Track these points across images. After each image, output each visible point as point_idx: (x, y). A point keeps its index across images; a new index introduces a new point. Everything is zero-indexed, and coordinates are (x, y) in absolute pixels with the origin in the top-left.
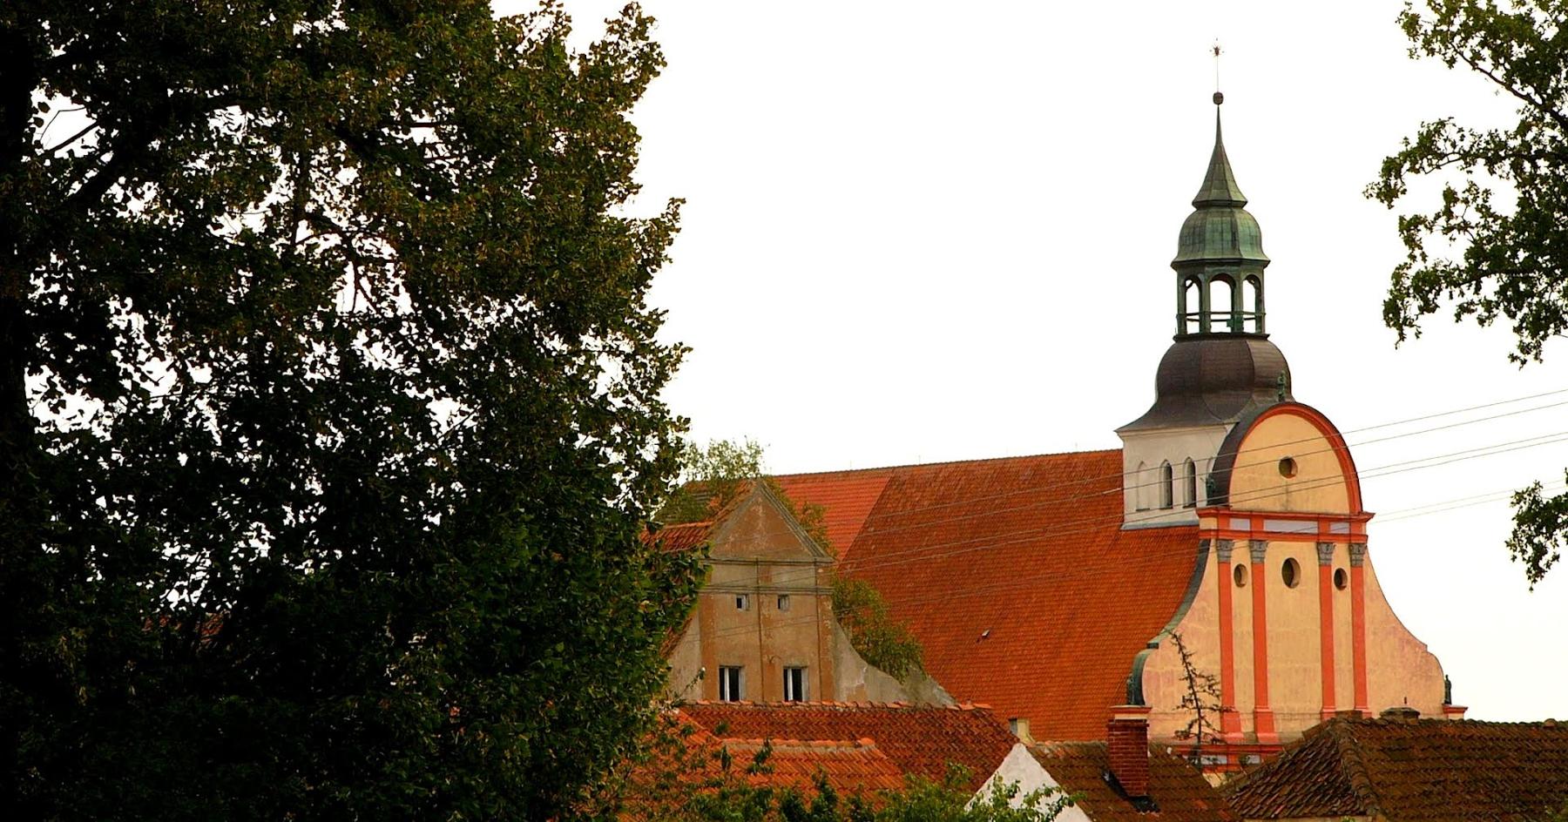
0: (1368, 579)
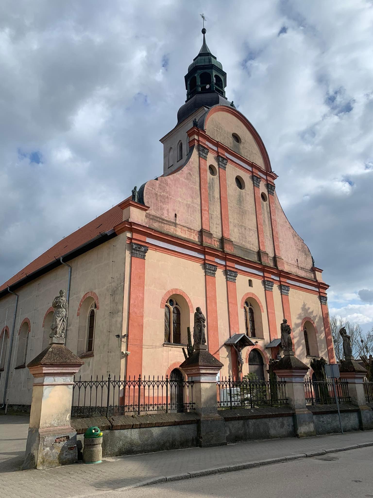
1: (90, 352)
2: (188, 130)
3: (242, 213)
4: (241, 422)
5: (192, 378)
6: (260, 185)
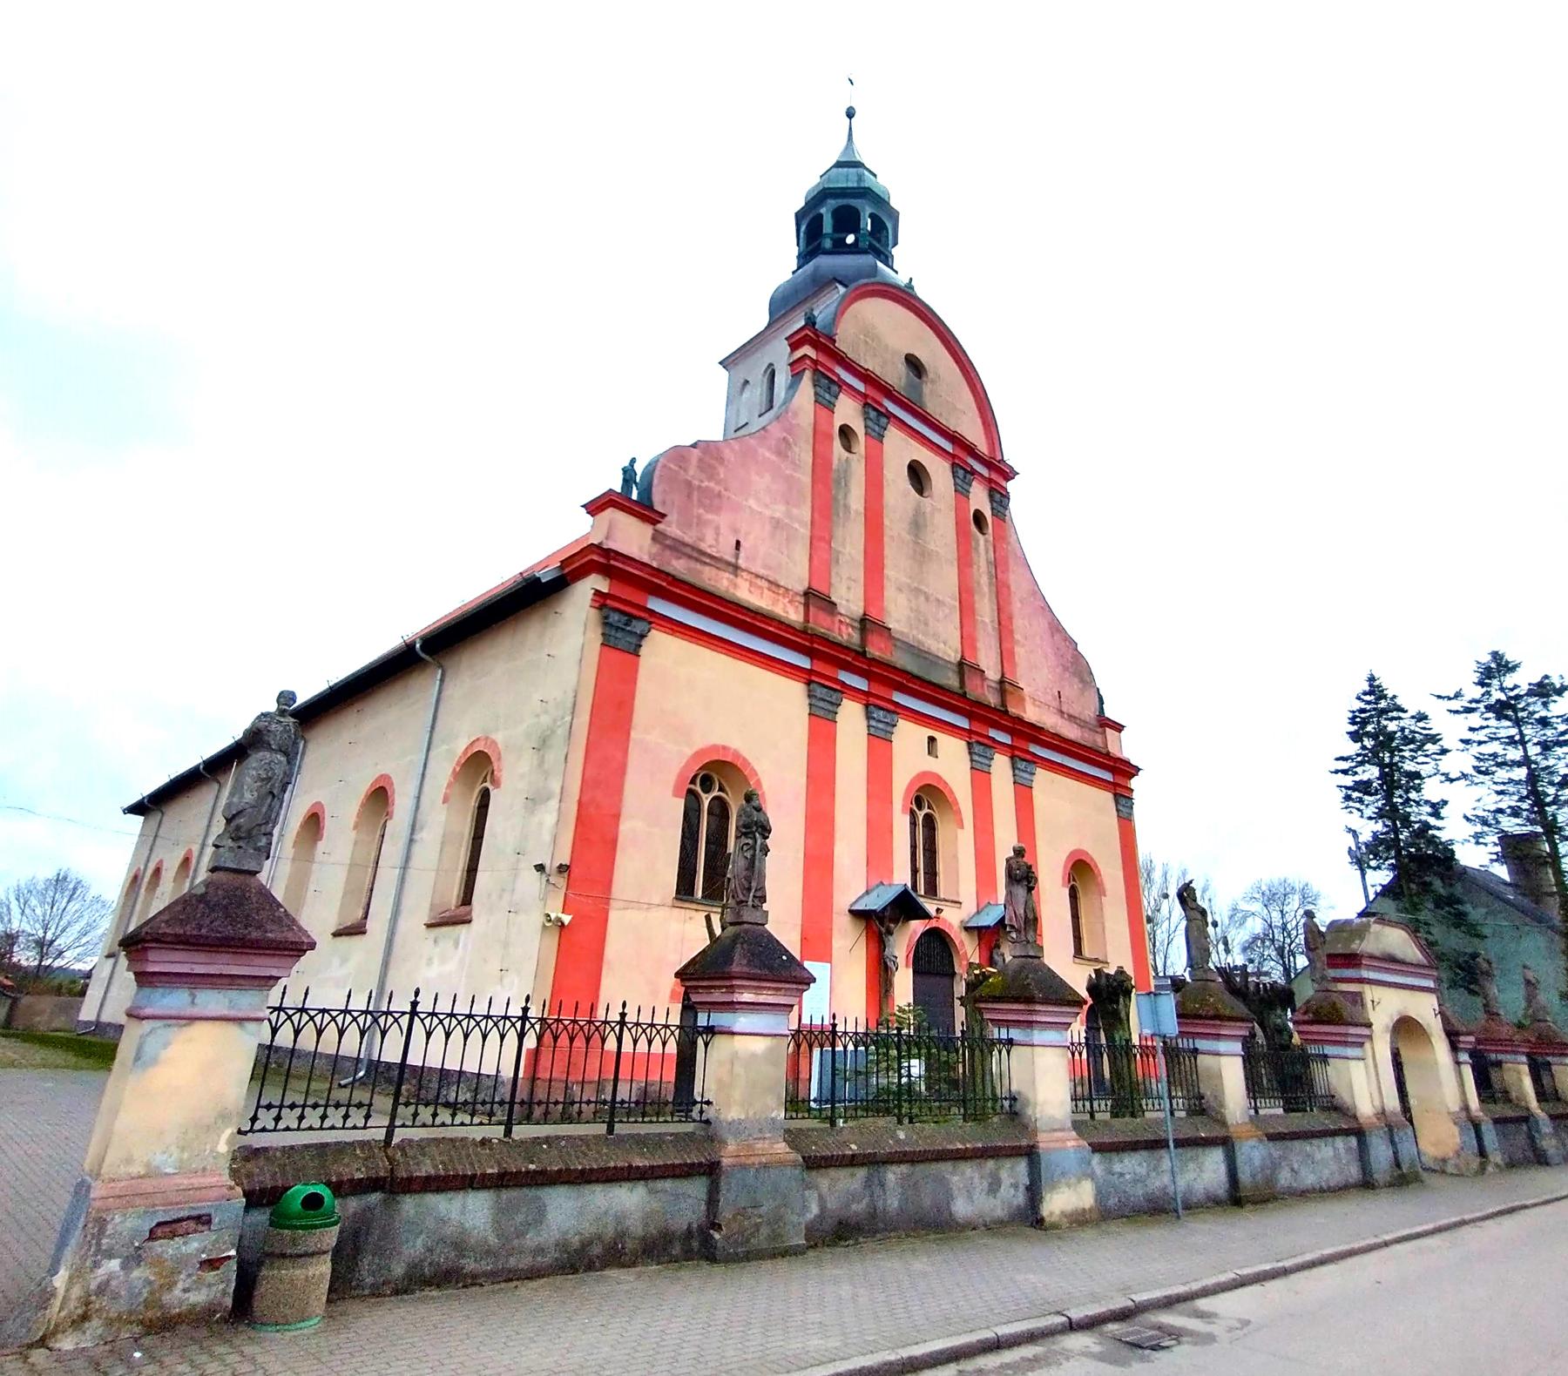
1: (467, 908)
3: (921, 555)
4: (861, 1173)
5: (709, 1016)
6: (971, 490)
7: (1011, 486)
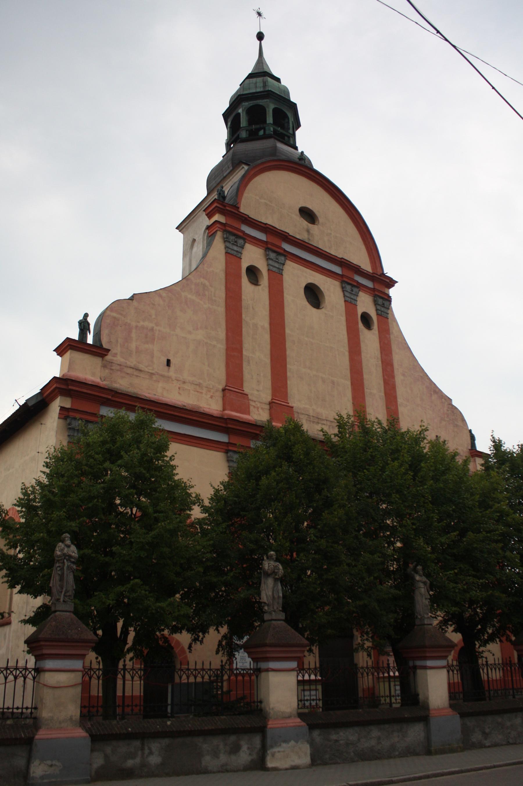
0: (393, 331)
2: (349, 276)
7: (392, 292)
